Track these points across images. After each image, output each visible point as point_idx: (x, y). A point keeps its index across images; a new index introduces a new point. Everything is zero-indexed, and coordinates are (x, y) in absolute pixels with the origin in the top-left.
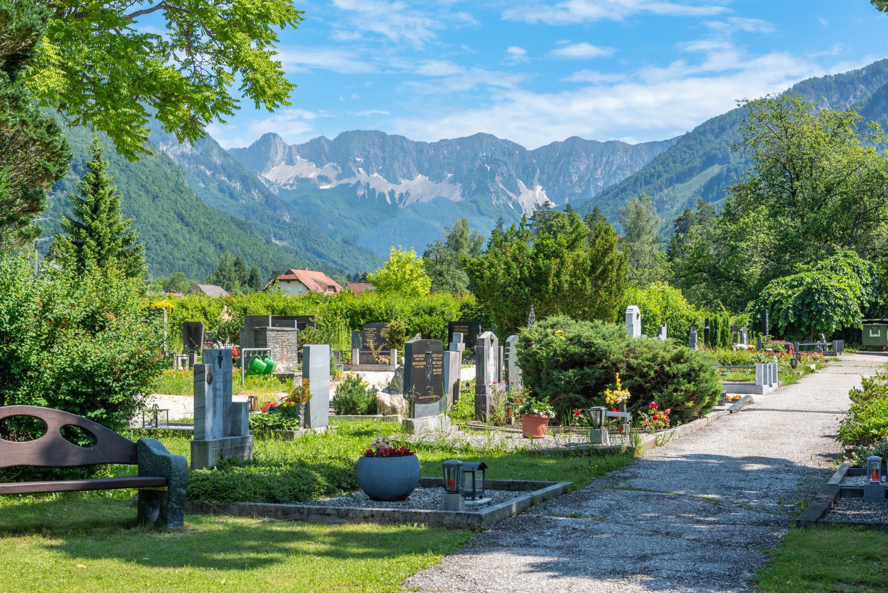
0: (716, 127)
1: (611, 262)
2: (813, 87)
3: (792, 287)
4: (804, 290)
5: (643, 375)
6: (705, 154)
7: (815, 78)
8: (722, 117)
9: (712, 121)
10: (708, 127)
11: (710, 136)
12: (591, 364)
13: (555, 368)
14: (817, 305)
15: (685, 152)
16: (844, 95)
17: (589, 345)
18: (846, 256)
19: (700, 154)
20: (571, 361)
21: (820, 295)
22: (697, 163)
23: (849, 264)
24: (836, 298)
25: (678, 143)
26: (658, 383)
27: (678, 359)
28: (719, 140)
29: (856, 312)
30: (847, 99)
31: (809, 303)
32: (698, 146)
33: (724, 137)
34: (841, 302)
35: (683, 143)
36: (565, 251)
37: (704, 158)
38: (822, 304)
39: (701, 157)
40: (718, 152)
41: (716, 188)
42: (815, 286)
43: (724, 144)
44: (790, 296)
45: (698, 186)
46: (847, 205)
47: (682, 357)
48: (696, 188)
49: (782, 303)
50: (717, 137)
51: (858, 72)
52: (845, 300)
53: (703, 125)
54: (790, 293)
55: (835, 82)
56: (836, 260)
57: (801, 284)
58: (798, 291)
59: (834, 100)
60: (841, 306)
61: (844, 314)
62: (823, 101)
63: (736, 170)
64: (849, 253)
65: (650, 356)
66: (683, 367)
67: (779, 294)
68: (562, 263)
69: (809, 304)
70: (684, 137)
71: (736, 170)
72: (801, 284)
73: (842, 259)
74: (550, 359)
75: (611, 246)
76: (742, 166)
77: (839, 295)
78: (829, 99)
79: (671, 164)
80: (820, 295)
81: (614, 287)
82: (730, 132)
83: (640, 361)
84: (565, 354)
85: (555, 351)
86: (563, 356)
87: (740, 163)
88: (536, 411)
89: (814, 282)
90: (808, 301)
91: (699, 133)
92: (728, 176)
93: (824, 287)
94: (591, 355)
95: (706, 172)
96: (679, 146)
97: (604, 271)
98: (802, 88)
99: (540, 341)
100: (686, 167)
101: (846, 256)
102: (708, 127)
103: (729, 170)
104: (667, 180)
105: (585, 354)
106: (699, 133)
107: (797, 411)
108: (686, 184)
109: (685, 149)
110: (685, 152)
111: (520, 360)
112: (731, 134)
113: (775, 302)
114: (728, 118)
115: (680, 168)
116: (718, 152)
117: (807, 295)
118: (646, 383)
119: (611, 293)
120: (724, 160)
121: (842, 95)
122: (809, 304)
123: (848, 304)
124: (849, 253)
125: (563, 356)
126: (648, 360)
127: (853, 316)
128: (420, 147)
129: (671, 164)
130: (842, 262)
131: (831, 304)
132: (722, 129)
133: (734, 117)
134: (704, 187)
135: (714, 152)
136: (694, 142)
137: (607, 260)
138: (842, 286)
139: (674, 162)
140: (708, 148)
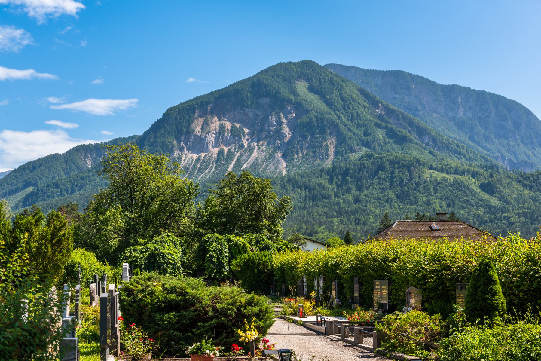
0: (31, 167)
1: (64, 235)
2: (83, 149)
3: (142, 253)
4: (149, 254)
5: (226, 316)
6: (24, 181)
7: (84, 145)
8: (34, 162)
9: (29, 164)
10: (26, 167)
11: (27, 171)
12: (186, 308)
13: (156, 312)
14: (158, 263)
15: (14, 179)
16: (99, 155)
17: (183, 293)
18: (168, 235)
19: (22, 180)
20: (170, 306)
21: (159, 257)
22: (20, 185)
23: (170, 240)
24: (169, 259)
25: (10, 174)
26: (237, 321)
27: (250, 303)
28: (32, 174)
29: (179, 267)
30: (100, 156)
31: (153, 262)
32: (21, 177)
33: (35, 172)
34: (171, 261)
35: (12, 174)
36: (33, 227)
37: (24, 183)
38: (161, 262)
39: (23, 182)
40: (32, 180)
41: (31, 199)
42: (157, 252)
43: (35, 176)
44: (141, 258)
45: (20, 198)
46: (163, 208)
47: (253, 302)
48: (19, 199)
49: (137, 262)
50: (31, 172)
51: (106, 143)
52: (173, 260)
53: (24, 165)
54: (142, 256)
55: (95, 147)
56: (163, 238)
57: (148, 251)
58: (146, 255)
59: (94, 156)
60: (171, 264)
61: (173, 268)
62: (88, 157)
63: (42, 190)
64: (170, 234)
65: (231, 301)
66: (256, 309)
67: (135, 257)
68: (31, 235)
69: (153, 263)
70: (13, 171)
71: (42, 190)
72: (148, 251)
73: (166, 237)
74: (153, 305)
75: (64, 225)
76: (45, 188)
77: (170, 257)
78: (91, 155)
79: (6, 185)
80: (159, 257)
81: (65, 251)
82: (38, 170)
83: (224, 305)
84: (166, 301)
85: (158, 298)
86: (164, 302)
87: (44, 186)
88: (208, 352)
89: (156, 250)
90: (152, 260)
91: (21, 169)
92: (37, 193)
93: (162, 253)
94: (185, 301)
95: (25, 190)
96: (10, 176)
97: (59, 240)
98: (77, 149)
99: (143, 291)
100: (14, 187)
101: (168, 235)
102: (26, 167)
103: (38, 190)
104: (3, 193)
105: (180, 300)
106: (21, 169)
107: (277, 334)
108: (14, 196)
109: (13, 177)
110: (14, 179)
111: (223, 312)
112: (39, 171)
113: (133, 261)
114: (37, 162)
115: (10, 188)
116: (32, 180)
117: (152, 257)
118: (228, 321)
119: (63, 255)
120: (35, 184)
121: (98, 154)
122: (153, 263)
123: (175, 263)
124: (170, 234)
125: (164, 302)
126: (229, 304)
127: (178, 269)
128: (443, 86)
129: (6, 185)
130: (166, 239)
131: (166, 262)
132: (34, 168)
133: (41, 162)
134: (24, 198)
135: (29, 180)
136: (18, 174)
137: (61, 233)
138: (171, 252)
139: (7, 184)
140: (26, 178)
